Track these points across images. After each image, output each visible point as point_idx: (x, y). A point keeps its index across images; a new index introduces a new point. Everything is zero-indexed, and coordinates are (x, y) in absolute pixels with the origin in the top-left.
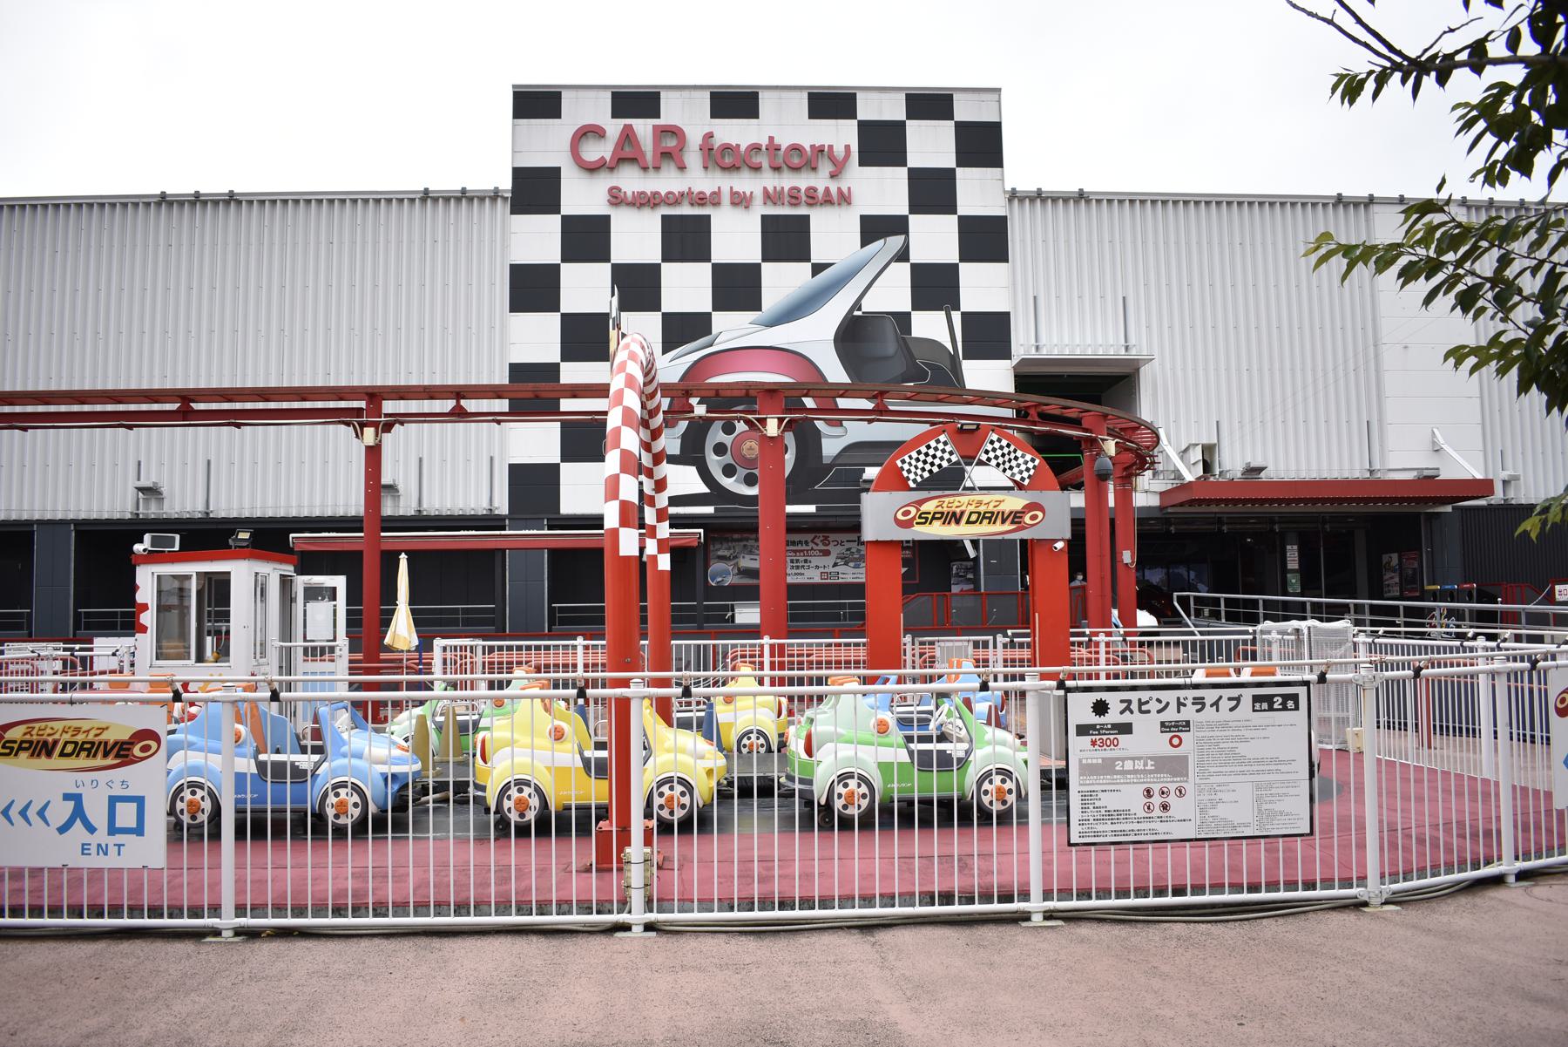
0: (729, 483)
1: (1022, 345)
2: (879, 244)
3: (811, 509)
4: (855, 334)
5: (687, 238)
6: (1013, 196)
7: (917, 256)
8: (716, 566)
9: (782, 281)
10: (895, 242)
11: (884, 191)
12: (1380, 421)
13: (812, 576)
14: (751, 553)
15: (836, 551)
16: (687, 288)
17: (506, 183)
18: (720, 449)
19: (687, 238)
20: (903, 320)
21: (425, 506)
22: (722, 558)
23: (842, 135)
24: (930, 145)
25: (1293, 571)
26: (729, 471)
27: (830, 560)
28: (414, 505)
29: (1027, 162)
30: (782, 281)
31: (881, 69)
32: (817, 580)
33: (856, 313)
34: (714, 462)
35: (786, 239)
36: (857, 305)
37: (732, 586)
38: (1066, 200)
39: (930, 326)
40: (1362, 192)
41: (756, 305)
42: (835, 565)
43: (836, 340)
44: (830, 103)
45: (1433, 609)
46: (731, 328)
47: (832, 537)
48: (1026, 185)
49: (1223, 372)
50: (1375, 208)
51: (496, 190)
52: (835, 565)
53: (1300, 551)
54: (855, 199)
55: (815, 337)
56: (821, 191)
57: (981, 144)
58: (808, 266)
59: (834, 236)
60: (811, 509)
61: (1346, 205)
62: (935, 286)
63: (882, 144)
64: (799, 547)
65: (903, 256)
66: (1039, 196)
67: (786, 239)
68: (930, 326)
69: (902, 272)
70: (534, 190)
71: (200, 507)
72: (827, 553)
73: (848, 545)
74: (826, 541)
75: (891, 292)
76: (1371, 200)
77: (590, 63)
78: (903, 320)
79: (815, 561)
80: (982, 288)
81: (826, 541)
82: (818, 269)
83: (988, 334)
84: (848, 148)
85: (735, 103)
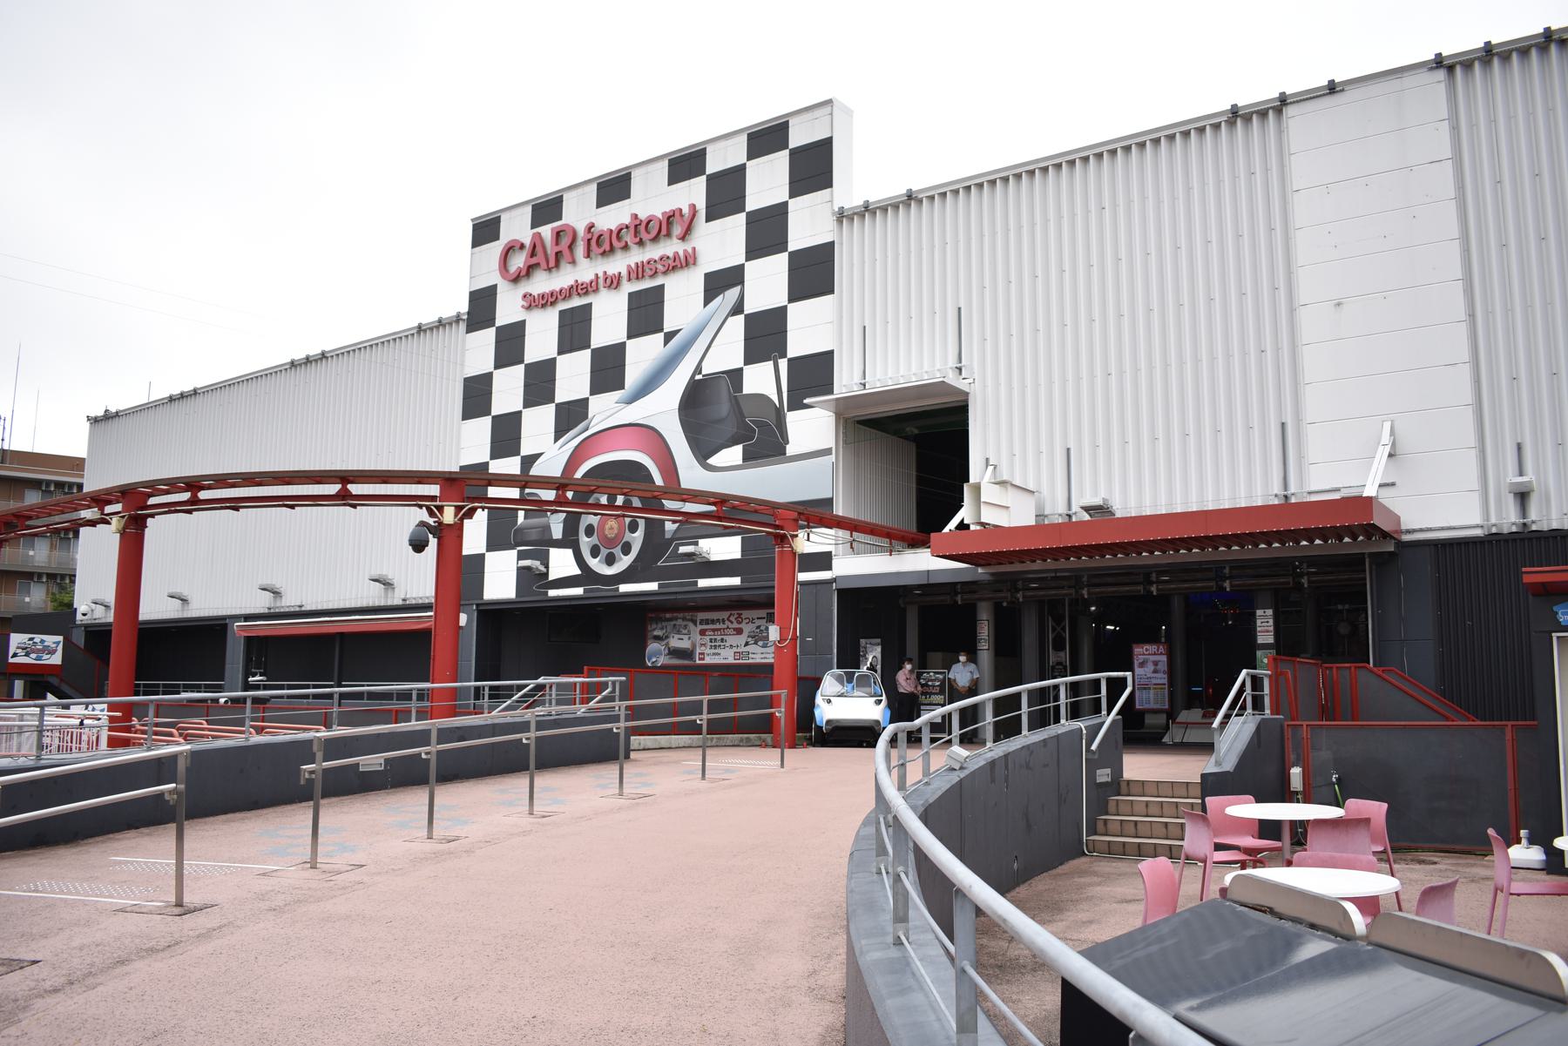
0: (596, 564)
1: (846, 382)
2: (719, 299)
3: (652, 586)
4: (697, 397)
5: (574, 331)
6: (842, 216)
7: (749, 308)
8: (653, 646)
9: (643, 354)
10: (732, 294)
11: (722, 242)
12: (1298, 420)
13: (726, 656)
14: (679, 632)
15: (747, 628)
16: (573, 376)
17: (464, 307)
18: (590, 531)
19: (574, 331)
20: (736, 376)
21: (1292, 489)
22: (657, 638)
23: (694, 192)
24: (767, 182)
25: (1265, 646)
26: (595, 552)
27: (742, 639)
28: (1277, 488)
29: (855, 180)
30: (643, 354)
31: (716, 117)
32: (731, 660)
33: (698, 377)
34: (585, 542)
35: (646, 313)
36: (698, 370)
37: (663, 667)
38: (896, 207)
39: (761, 380)
40: (1267, 92)
41: (620, 385)
42: (747, 644)
43: (680, 409)
44: (685, 165)
45: (145, 704)
46: (606, 410)
47: (745, 614)
48: (854, 201)
49: (1143, 365)
50: (1289, 111)
51: (458, 315)
52: (747, 644)
53: (1276, 617)
54: (701, 259)
55: (661, 408)
56: (681, 254)
57: (813, 168)
58: (661, 335)
59: (683, 300)
60: (652, 586)
61: (1247, 119)
62: (765, 335)
63: (726, 193)
64: (717, 626)
65: (738, 309)
66: (867, 210)
67: (646, 313)
68: (761, 380)
69: (737, 324)
70: (481, 307)
71: (1061, 508)
72: (739, 632)
73: (758, 622)
74: (739, 620)
75: (726, 350)
76: (1284, 100)
77: (510, 188)
78: (736, 376)
79: (732, 640)
80: (809, 329)
81: (739, 620)
82: (669, 337)
83: (812, 376)
84: (693, 207)
85: (614, 188)
